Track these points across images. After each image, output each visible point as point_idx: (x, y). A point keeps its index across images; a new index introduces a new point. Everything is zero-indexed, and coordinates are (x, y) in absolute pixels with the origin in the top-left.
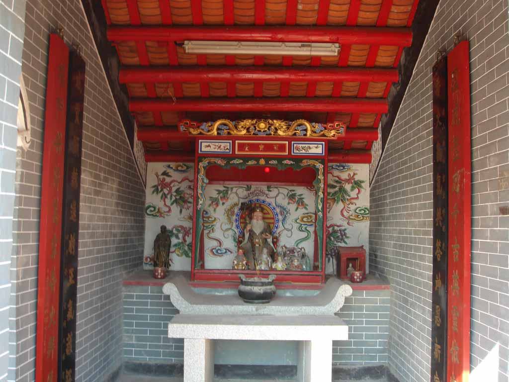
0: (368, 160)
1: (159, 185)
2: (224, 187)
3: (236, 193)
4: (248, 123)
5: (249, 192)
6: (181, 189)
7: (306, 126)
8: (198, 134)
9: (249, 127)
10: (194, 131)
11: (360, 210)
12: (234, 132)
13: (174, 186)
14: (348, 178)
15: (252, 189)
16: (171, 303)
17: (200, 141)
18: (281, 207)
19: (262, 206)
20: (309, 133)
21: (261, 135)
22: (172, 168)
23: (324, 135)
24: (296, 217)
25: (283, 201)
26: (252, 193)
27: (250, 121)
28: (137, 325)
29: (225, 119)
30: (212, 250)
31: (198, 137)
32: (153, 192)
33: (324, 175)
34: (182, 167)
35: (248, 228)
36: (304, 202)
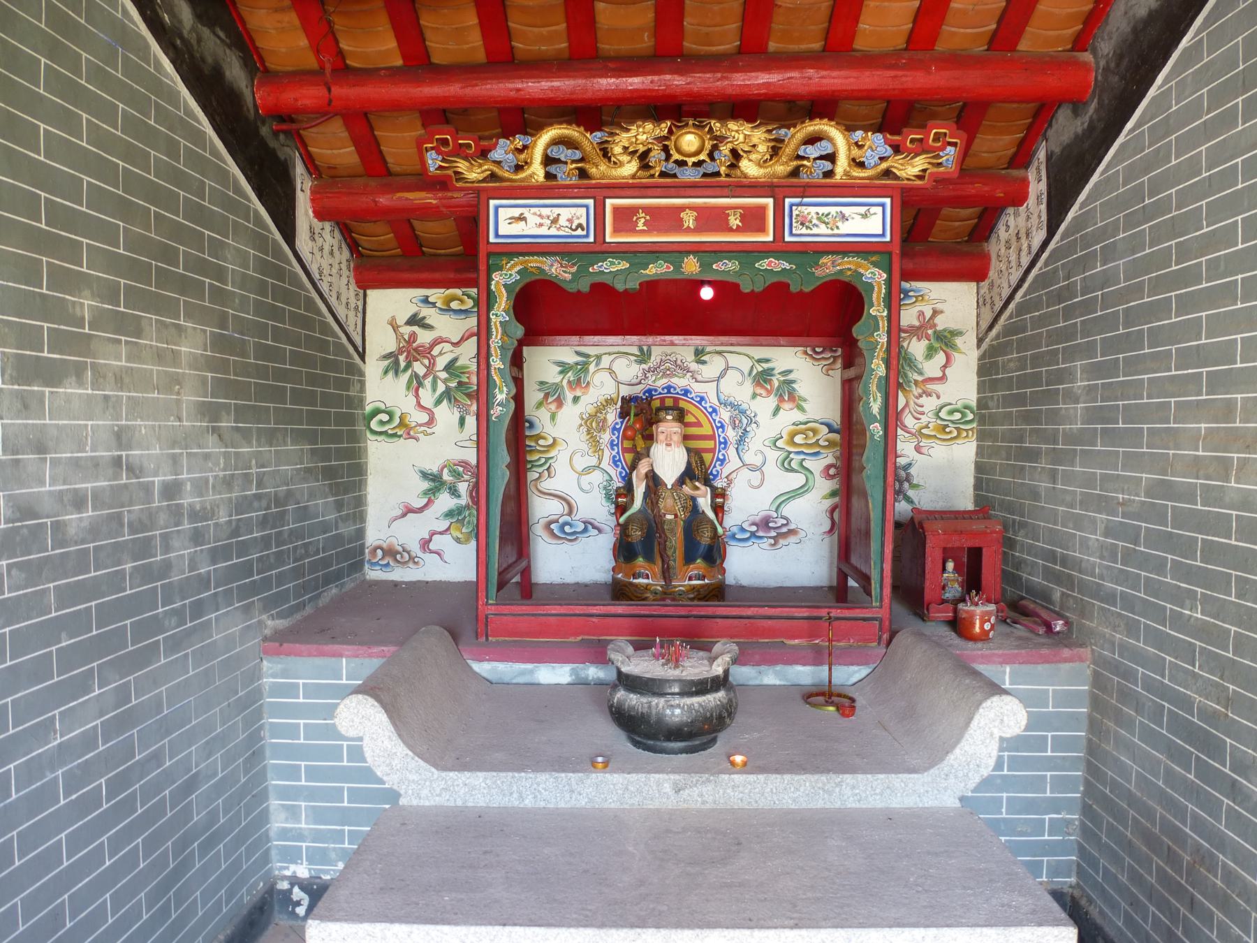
0: (977, 273)
1: (400, 351)
2: (578, 353)
3: (610, 370)
4: (643, 133)
5: (644, 366)
6: (458, 364)
7: (831, 140)
9: (649, 150)
10: (470, 170)
11: (951, 412)
12: (600, 170)
13: (441, 354)
14: (917, 324)
15: (653, 358)
17: (492, 203)
19: (682, 404)
20: (842, 164)
21: (689, 175)
22: (434, 304)
23: (887, 173)
24: (774, 434)
25: (738, 388)
26: (653, 370)
28: (312, 774)
29: (569, 123)
30: (548, 526)
32: (386, 372)
33: (889, 306)
34: (462, 301)
35: (643, 468)
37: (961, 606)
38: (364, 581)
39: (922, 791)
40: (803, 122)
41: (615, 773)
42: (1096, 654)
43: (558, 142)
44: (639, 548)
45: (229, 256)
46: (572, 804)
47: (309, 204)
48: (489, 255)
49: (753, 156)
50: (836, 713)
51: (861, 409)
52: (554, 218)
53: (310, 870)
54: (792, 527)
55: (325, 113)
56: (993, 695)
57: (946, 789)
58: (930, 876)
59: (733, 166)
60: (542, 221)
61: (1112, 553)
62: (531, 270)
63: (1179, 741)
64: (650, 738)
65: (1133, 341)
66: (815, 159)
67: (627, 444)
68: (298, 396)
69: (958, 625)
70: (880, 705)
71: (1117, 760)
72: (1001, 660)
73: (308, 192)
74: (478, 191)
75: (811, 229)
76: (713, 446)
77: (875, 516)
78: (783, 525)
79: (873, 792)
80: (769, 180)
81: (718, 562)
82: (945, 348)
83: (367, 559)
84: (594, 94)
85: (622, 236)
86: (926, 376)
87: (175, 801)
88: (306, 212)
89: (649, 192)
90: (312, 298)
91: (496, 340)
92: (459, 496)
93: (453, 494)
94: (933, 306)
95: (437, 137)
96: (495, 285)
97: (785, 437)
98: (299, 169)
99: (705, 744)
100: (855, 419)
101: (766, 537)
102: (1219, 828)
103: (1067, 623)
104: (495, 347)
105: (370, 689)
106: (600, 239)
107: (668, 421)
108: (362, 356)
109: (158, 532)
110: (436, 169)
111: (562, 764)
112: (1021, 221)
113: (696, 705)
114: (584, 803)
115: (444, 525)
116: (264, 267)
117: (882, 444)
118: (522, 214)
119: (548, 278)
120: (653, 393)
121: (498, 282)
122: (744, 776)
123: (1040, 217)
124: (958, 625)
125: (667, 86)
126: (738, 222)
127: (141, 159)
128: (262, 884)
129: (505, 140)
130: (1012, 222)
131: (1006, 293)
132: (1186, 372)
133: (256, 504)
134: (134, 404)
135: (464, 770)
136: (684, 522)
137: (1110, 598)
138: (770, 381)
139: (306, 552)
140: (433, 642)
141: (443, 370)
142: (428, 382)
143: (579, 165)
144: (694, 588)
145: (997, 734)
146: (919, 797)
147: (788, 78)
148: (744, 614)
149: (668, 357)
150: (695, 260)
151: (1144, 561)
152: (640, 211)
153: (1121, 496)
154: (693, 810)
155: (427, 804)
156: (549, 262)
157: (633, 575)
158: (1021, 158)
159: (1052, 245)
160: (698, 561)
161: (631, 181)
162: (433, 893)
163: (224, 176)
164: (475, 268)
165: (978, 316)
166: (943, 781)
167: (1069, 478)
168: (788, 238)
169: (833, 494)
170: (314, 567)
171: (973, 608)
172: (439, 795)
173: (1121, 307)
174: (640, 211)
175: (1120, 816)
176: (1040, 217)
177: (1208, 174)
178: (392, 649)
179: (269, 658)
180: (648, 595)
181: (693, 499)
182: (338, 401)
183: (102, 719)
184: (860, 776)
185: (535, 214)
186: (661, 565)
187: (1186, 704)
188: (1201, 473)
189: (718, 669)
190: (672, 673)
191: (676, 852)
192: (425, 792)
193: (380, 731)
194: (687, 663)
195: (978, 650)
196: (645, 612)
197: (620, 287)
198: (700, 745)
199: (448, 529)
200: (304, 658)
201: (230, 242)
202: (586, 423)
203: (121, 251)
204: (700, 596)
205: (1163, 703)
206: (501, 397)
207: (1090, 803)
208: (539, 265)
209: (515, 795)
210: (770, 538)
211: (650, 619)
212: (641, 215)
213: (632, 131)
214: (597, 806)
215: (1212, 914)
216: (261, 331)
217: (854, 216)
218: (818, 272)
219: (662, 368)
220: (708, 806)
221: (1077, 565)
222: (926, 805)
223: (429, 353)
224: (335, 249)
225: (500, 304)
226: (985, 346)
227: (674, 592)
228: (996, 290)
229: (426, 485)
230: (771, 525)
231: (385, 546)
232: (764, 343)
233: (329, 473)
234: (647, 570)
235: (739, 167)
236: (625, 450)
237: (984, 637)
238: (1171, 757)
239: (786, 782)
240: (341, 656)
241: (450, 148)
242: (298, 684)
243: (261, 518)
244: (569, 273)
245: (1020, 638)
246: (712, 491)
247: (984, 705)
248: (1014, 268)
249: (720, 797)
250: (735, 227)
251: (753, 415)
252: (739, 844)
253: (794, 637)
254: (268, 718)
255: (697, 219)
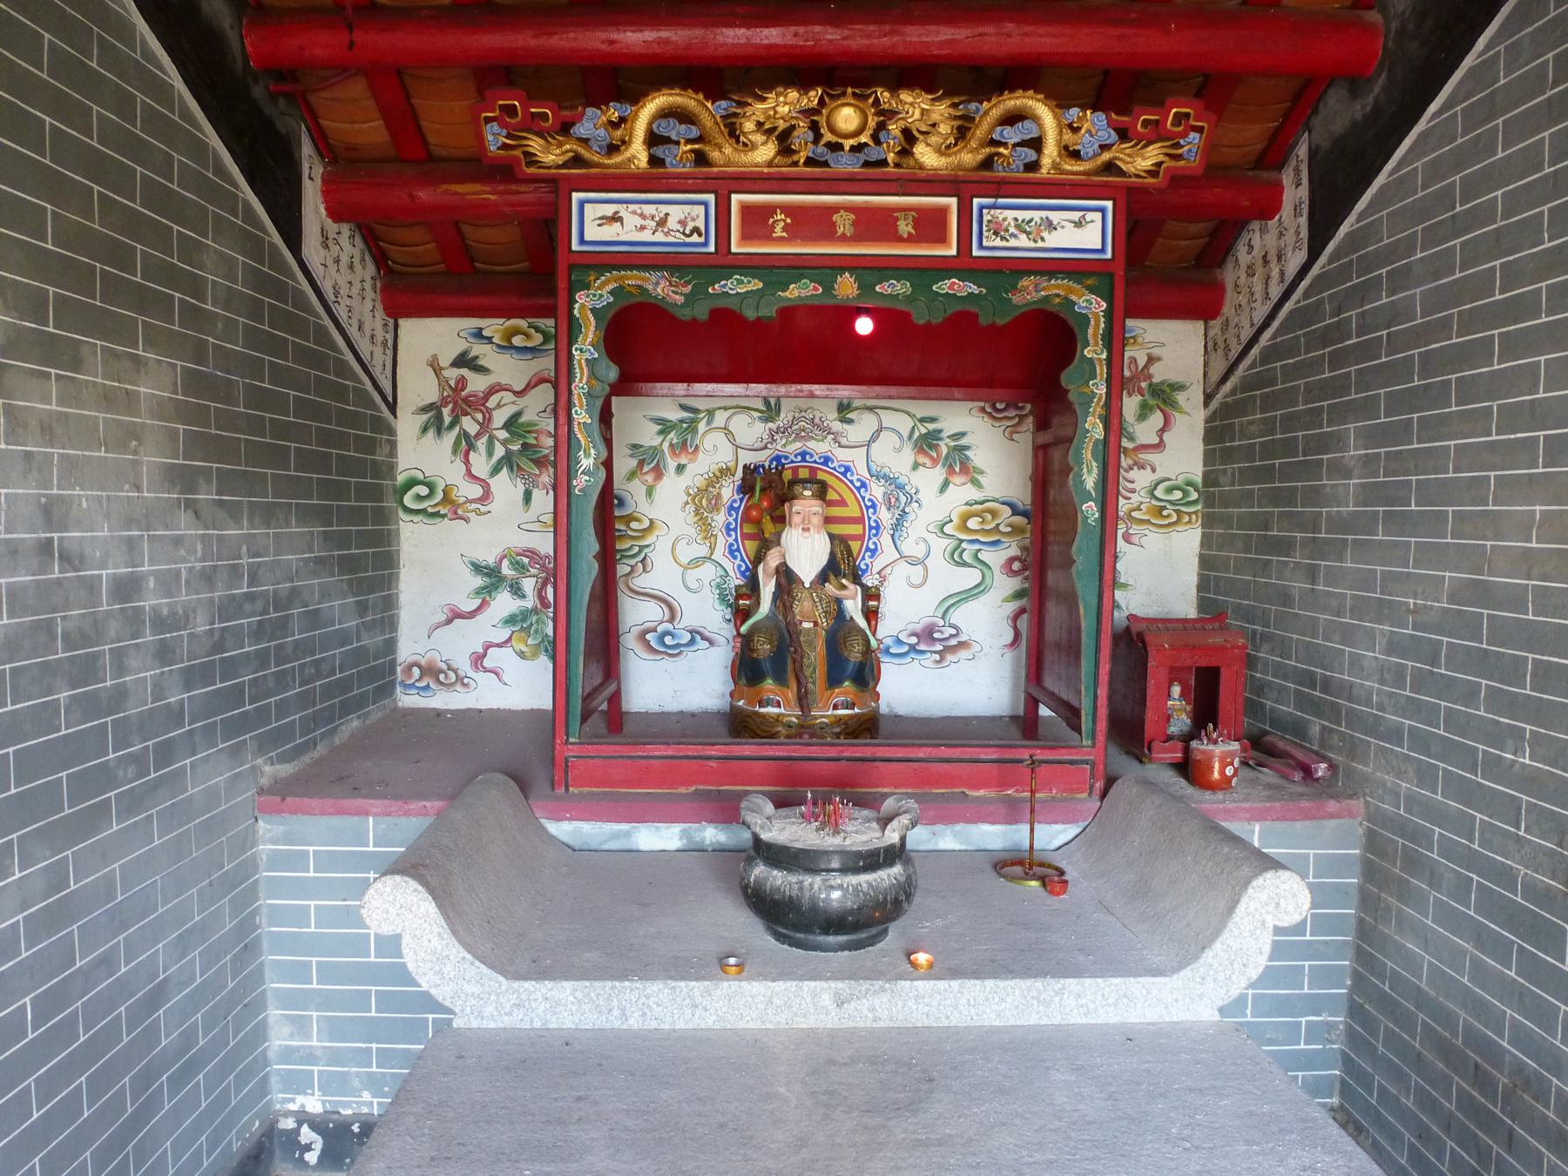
2: (684, 408)
4: (784, 104)
5: (771, 425)
6: (523, 419)
7: (1036, 119)
8: (565, 165)
9: (793, 128)
12: (724, 154)
13: (499, 406)
15: (783, 415)
16: (403, 966)
17: (576, 196)
18: (886, 478)
19: (821, 476)
20: (1051, 150)
21: (845, 164)
22: (489, 340)
23: (1110, 168)
24: (941, 516)
25: (894, 455)
27: (793, 95)
28: (327, 973)
30: (642, 637)
31: (567, 178)
32: (425, 430)
34: (527, 336)
35: (773, 560)
36: (968, 458)
37: (1194, 744)
38: (396, 709)
39: (1170, 1000)
40: (1001, 94)
41: (754, 980)
42: (1372, 808)
43: (665, 114)
44: (767, 666)
45: (208, 263)
46: (696, 1023)
47: (320, 198)
48: (571, 268)
49: (933, 139)
50: (1042, 889)
51: (1071, 483)
52: (661, 219)
53: (324, 1102)
54: (963, 638)
55: (343, 69)
56: (1266, 870)
57: (1201, 997)
58: (1198, 1125)
59: (906, 152)
60: (643, 223)
61: (1399, 676)
62: (629, 289)
63: (1493, 926)
64: (799, 931)
65: (1439, 395)
66: (1015, 145)
67: (748, 529)
68: (307, 461)
69: (1189, 769)
70: (1098, 878)
71: (1400, 948)
72: (1248, 815)
73: (319, 181)
74: (552, 181)
75: (1008, 241)
76: (861, 532)
77: (1087, 624)
78: (952, 636)
79: (1104, 1003)
80: (953, 172)
81: (871, 685)
82: (1162, 406)
83: (399, 679)
84: (716, 49)
85: (752, 246)
86: (1139, 442)
87: (134, 1020)
88: (317, 207)
89: (791, 185)
90: (325, 326)
91: (580, 384)
92: (524, 596)
93: (516, 594)
94: (1149, 351)
95: (501, 102)
96: (579, 309)
97: (956, 520)
98: (307, 149)
99: (873, 937)
100: (1051, 498)
101: (930, 652)
102: (1552, 1043)
103: (1332, 767)
104: (579, 394)
105: (410, 866)
106: (723, 249)
107: (805, 498)
108: (393, 407)
109: (107, 647)
110: (499, 149)
111: (680, 968)
112: (1271, 240)
113: (864, 885)
114: (711, 1022)
115: (504, 634)
116: (258, 281)
117: (1098, 530)
118: (617, 212)
119: (652, 301)
120: (783, 461)
121: (583, 305)
122: (932, 982)
123: (1298, 233)
124: (1189, 769)
125: (816, 41)
126: (910, 229)
127: (80, 117)
128: (257, 1124)
129: (594, 109)
130: (1256, 240)
131: (1247, 334)
132: (1512, 436)
133: (248, 607)
134: (69, 464)
135: (545, 978)
136: (826, 631)
137: (1395, 735)
138: (936, 447)
139: (317, 671)
140: (495, 795)
141: (502, 428)
142: (481, 444)
143: (696, 146)
144: (839, 720)
145: (1271, 922)
146: (1166, 1007)
147: (980, 35)
148: (913, 756)
149: (803, 414)
150: (852, 280)
151: (1445, 688)
152: (778, 211)
153: (1412, 601)
154: (862, 1029)
155: (492, 1025)
156: (654, 279)
157: (760, 703)
158: (1274, 155)
159: (1316, 270)
160: (846, 683)
161: (766, 170)
162: (508, 1164)
163: (199, 150)
164: (551, 291)
165: (1206, 364)
166: (1198, 986)
167: (1333, 577)
168: (976, 253)
169: (1019, 595)
170: (328, 692)
171: (1211, 747)
172: (509, 1014)
173: (1416, 351)
174: (778, 211)
175: (1405, 1021)
176: (1298, 233)
177: (1552, 169)
178: (438, 804)
179: (267, 817)
180: (780, 729)
181: (839, 601)
182: (358, 468)
183: (25, 914)
184: (1087, 981)
185: (634, 213)
186: (795, 689)
187: (1505, 877)
188: (1535, 571)
189: (892, 836)
190: (831, 841)
191: (845, 1094)
192: (490, 1009)
193: (425, 925)
194: (849, 827)
195: (1220, 802)
196: (781, 754)
197: (750, 314)
198: (868, 938)
199: (510, 639)
200: (314, 817)
201: (210, 243)
202: (693, 500)
203: (50, 247)
204: (848, 731)
205: (1471, 875)
206: (586, 462)
207: (1361, 1001)
208: (639, 283)
209: (616, 1013)
210: (935, 652)
211: (787, 763)
212: (779, 217)
213: (770, 101)
214: (729, 1027)
215: (1540, 1156)
216: (255, 368)
217: (1064, 223)
218: (1016, 299)
219: (794, 428)
220: (881, 1024)
221: (1347, 691)
222: (1175, 1019)
223: (483, 405)
224: (356, 261)
225: (586, 335)
226: (1215, 404)
227: (814, 725)
228: (1232, 331)
229: (479, 581)
230: (936, 635)
231: (423, 662)
232: (932, 396)
233: (349, 565)
234: (778, 695)
235: (912, 154)
236: (745, 537)
237: (1225, 784)
238: (1480, 945)
239: (988, 990)
240: (367, 814)
241: (519, 119)
242: (308, 851)
243: (255, 627)
244: (681, 294)
245: (1269, 786)
246: (863, 591)
247: (1254, 883)
248: (1259, 301)
249: (898, 1012)
250: (905, 236)
251: (914, 491)
252: (931, 1080)
253: (976, 787)
254: (265, 900)
255: (854, 224)
